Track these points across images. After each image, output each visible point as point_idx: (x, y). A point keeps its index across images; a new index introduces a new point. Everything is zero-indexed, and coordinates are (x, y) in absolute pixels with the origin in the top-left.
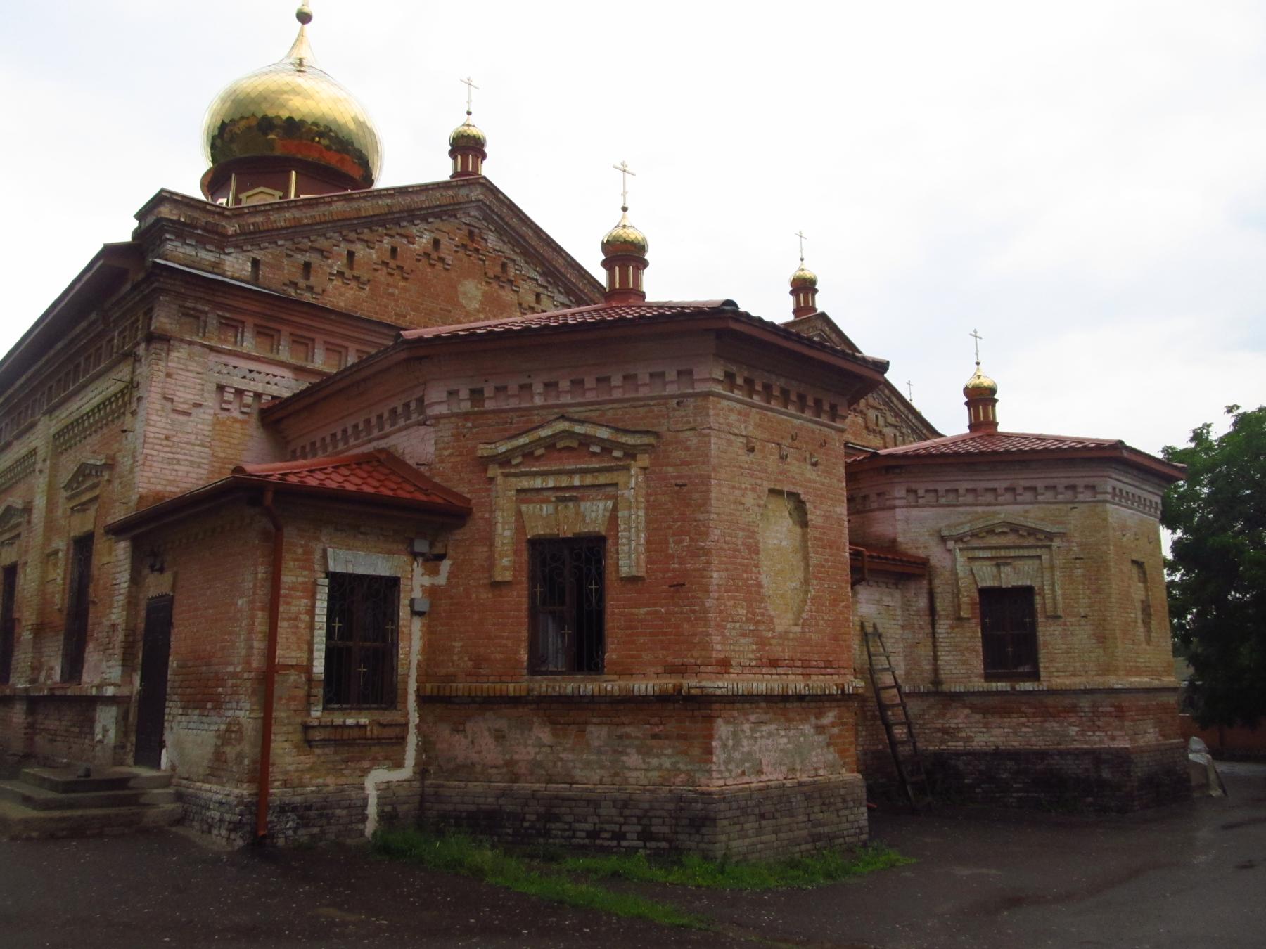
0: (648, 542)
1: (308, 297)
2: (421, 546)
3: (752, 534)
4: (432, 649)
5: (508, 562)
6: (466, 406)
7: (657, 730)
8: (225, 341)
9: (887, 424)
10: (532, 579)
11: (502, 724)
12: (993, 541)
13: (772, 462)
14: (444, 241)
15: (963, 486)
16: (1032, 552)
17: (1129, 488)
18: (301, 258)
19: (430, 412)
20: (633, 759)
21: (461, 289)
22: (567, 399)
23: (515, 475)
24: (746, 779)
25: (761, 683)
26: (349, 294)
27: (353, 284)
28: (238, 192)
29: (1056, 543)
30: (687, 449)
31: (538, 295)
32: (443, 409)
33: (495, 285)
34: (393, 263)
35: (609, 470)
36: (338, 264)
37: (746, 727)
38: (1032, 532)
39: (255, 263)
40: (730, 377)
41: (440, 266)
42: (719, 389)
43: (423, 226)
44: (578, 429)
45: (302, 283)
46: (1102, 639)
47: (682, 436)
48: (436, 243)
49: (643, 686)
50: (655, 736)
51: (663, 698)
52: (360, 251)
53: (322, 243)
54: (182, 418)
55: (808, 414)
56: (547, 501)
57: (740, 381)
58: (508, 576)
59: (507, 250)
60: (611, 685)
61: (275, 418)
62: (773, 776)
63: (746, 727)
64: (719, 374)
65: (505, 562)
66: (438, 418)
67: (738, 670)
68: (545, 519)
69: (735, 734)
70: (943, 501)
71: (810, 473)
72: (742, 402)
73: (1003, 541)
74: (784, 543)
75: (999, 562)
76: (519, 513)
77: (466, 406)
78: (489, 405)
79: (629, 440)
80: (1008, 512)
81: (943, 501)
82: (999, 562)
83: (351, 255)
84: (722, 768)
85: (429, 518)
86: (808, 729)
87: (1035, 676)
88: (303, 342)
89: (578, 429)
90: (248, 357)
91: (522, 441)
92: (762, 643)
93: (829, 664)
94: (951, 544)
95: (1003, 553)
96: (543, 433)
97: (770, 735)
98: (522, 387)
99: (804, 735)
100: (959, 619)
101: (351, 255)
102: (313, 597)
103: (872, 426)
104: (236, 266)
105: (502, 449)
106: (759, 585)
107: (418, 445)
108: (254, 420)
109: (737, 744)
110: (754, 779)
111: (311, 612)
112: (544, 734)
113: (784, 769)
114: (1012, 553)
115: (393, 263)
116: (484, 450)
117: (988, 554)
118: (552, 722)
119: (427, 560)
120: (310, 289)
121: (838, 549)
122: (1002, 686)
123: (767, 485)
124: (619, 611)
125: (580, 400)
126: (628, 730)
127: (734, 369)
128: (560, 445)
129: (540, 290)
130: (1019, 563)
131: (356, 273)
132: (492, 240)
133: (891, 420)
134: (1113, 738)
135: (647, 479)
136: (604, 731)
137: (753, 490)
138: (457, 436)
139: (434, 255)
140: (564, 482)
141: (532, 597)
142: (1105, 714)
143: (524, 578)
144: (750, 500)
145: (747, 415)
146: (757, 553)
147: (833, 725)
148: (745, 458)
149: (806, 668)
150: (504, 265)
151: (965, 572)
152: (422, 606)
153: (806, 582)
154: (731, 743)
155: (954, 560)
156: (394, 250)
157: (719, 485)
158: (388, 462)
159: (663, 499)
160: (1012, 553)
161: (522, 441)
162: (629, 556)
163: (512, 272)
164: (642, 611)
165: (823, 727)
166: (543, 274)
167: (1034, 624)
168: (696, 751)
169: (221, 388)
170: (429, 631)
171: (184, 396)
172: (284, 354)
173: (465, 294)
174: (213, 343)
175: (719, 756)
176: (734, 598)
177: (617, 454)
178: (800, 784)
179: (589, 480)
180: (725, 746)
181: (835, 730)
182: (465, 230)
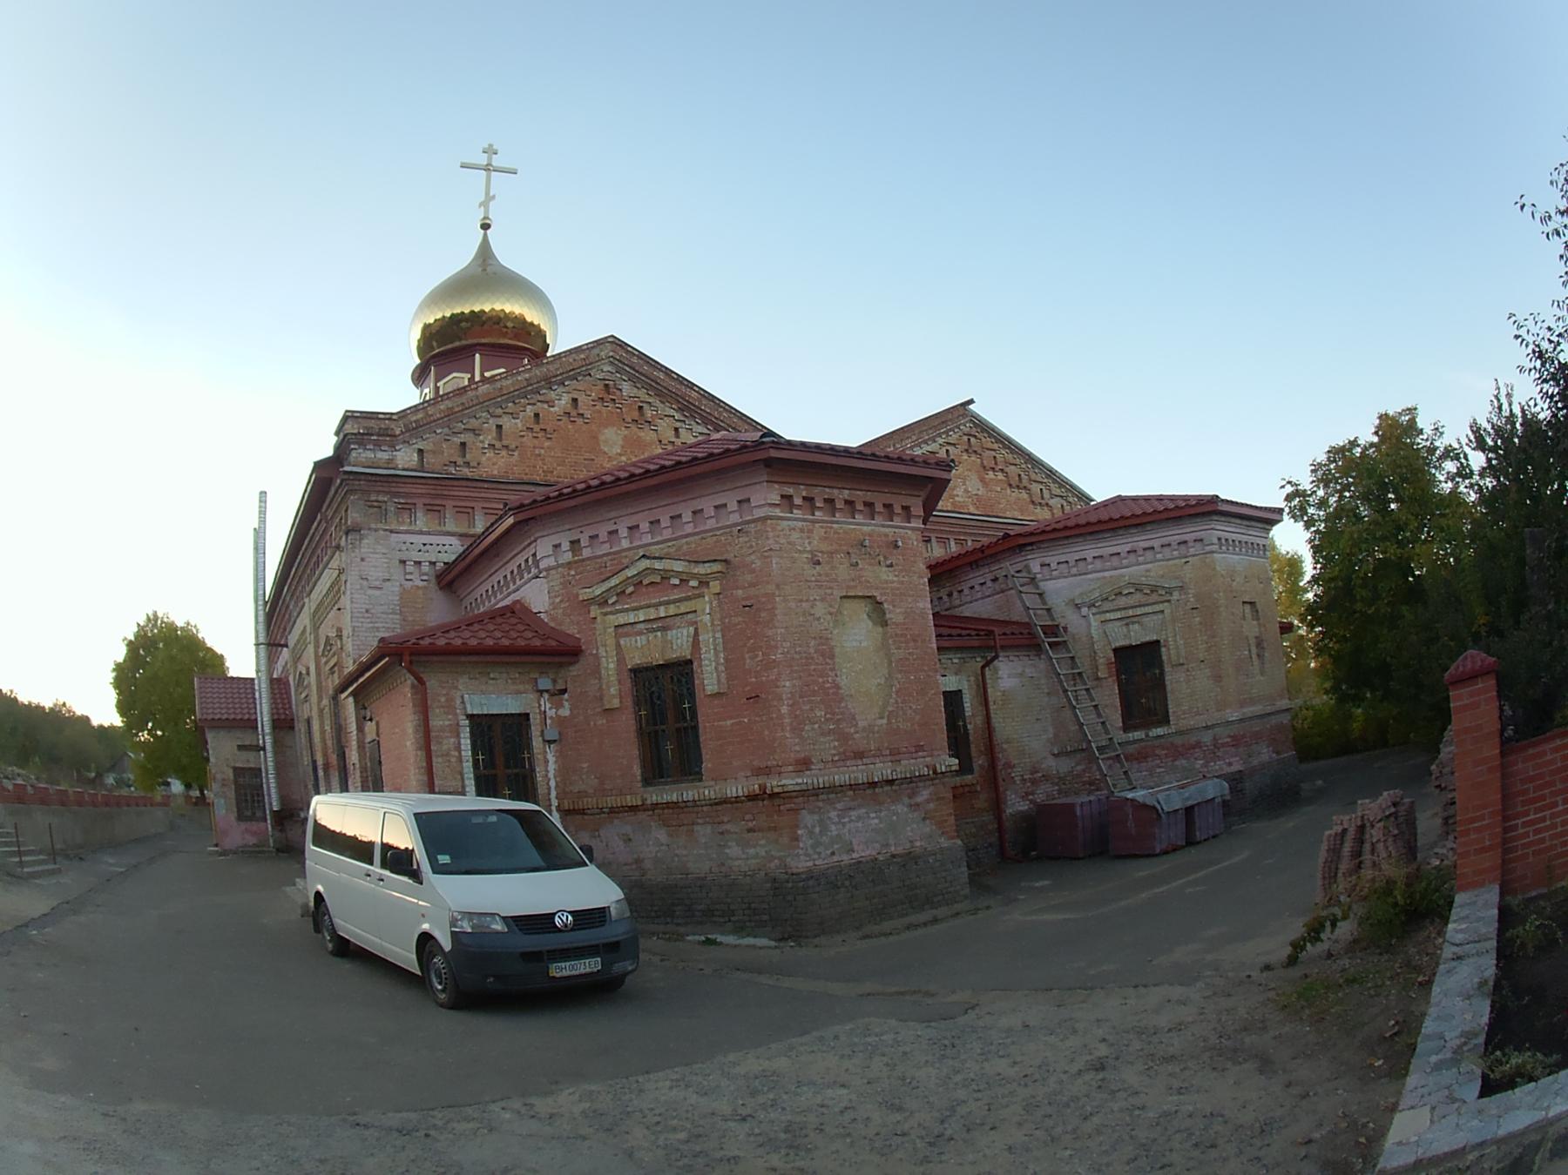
0: (726, 659)
1: (466, 472)
2: (545, 683)
3: (824, 640)
4: (564, 772)
5: (614, 689)
6: (568, 557)
7: (750, 825)
8: (403, 523)
9: (1053, 496)
10: (637, 703)
11: (628, 829)
12: (1122, 602)
13: (843, 571)
14: (582, 398)
15: (1090, 554)
16: (1157, 608)
17: (1234, 536)
18: (457, 440)
19: (542, 565)
20: (734, 850)
21: (602, 438)
22: (648, 539)
23: (611, 613)
24: (835, 858)
25: (841, 777)
26: (501, 462)
27: (504, 453)
28: (437, 380)
29: (1176, 595)
30: (753, 571)
31: (676, 430)
32: (551, 562)
33: (634, 427)
34: (537, 428)
35: (688, 599)
36: (489, 438)
37: (833, 814)
38: (1154, 589)
39: (420, 451)
40: (787, 498)
41: (580, 421)
42: (778, 512)
43: (561, 389)
44: (657, 565)
45: (460, 461)
46: (1218, 678)
47: (748, 559)
48: (575, 400)
49: (734, 790)
50: (749, 831)
51: (752, 798)
52: (507, 422)
53: (474, 423)
54: (377, 593)
55: (879, 520)
56: (640, 633)
57: (798, 501)
58: (616, 703)
59: (642, 393)
60: (707, 790)
61: (452, 579)
62: (863, 852)
63: (833, 814)
64: (776, 499)
65: (613, 691)
66: (548, 569)
67: (821, 766)
68: (645, 650)
69: (821, 822)
70: (1074, 570)
71: (885, 574)
72: (804, 520)
73: (1131, 601)
74: (864, 644)
75: (1127, 621)
76: (618, 645)
77: (568, 557)
78: (586, 553)
79: (701, 569)
80: (1134, 571)
81: (1074, 570)
82: (1127, 621)
83: (499, 427)
84: (810, 851)
85: (553, 655)
86: (901, 808)
87: (1165, 721)
88: (466, 512)
89: (657, 565)
90: (421, 533)
91: (613, 582)
92: (844, 737)
93: (919, 748)
94: (1084, 610)
95: (1130, 613)
96: (630, 573)
97: (859, 818)
98: (610, 533)
99: (896, 814)
100: (1098, 679)
101: (499, 427)
102: (458, 736)
103: (1037, 499)
104: (405, 458)
105: (598, 592)
106: (838, 687)
107: (537, 596)
108: (433, 585)
109: (824, 830)
110: (845, 857)
111: (458, 748)
112: (661, 835)
113: (877, 846)
114: (1139, 611)
115: (537, 428)
116: (585, 594)
117: (1118, 615)
118: (665, 824)
119: (552, 695)
120: (467, 464)
121: (924, 641)
122: (1139, 735)
123: (838, 593)
124: (712, 725)
125: (659, 538)
126: (728, 827)
127: (790, 491)
128: (645, 582)
129: (678, 424)
130: (1145, 619)
131: (505, 443)
132: (626, 388)
133: (1057, 491)
134: (1230, 764)
135: (720, 603)
136: (709, 829)
137: (823, 600)
138: (566, 584)
139: (574, 413)
140: (652, 614)
141: (639, 719)
142: (1223, 745)
143: (629, 702)
144: (820, 609)
145: (810, 531)
146: (832, 657)
147: (928, 801)
148: (811, 572)
149: (895, 755)
150: (641, 408)
151: (1098, 634)
152: (552, 734)
153: (890, 677)
154: (817, 830)
155: (1089, 625)
156: (537, 415)
157: (785, 601)
158: (517, 613)
159: (736, 620)
160: (1139, 611)
161: (613, 582)
162: (709, 678)
163: (649, 413)
164: (729, 722)
165: (917, 805)
166: (680, 410)
167: (1162, 673)
168: (785, 840)
169: (403, 562)
170: (561, 756)
171: (375, 575)
172: (450, 526)
173: (606, 441)
174: (393, 527)
175: (806, 842)
176: (810, 702)
177: (693, 583)
178: (893, 856)
179: (672, 610)
180: (811, 833)
181: (932, 806)
182: (601, 385)
